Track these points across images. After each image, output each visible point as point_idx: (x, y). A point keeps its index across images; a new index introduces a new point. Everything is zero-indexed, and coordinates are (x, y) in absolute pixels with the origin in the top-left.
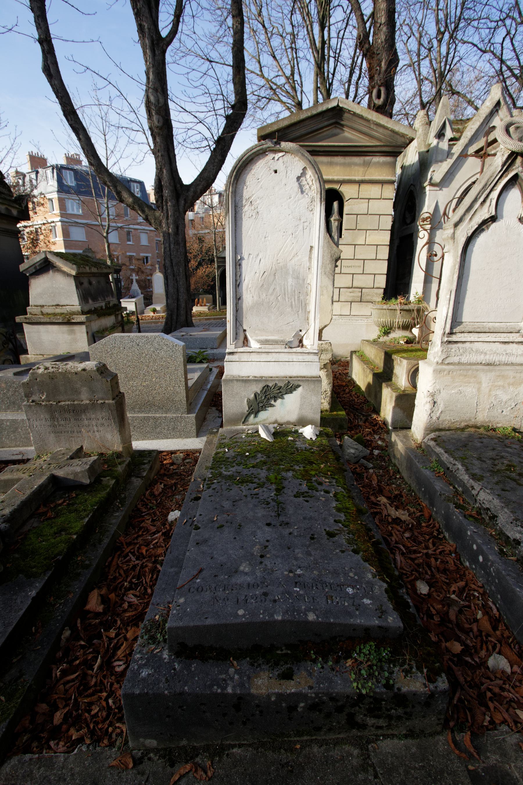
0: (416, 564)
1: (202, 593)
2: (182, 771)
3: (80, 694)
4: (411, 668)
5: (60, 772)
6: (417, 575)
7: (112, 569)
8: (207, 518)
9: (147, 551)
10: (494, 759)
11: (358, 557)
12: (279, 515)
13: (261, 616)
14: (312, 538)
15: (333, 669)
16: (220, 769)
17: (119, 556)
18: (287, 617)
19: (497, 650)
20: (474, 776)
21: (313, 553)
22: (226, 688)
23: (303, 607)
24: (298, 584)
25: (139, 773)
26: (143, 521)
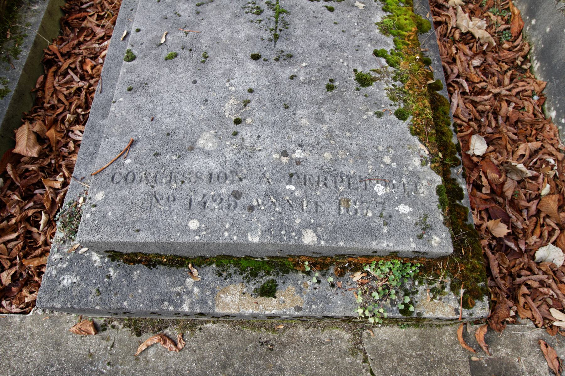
0: (478, 111)
1: (134, 185)
2: (149, 343)
3: (25, 256)
4: (443, 288)
5: (18, 332)
6: (476, 127)
7: (48, 93)
8: (149, 37)
9: (93, 68)
10: (503, 352)
11: (404, 126)
12: (276, 37)
13: (226, 234)
14: (330, 88)
15: (333, 285)
16: (192, 341)
17: (55, 74)
18: (268, 239)
19: (554, 238)
20: (475, 368)
21: (327, 118)
22: (180, 305)
23: (298, 221)
24: (295, 177)
25: (103, 339)
26: (84, 18)
